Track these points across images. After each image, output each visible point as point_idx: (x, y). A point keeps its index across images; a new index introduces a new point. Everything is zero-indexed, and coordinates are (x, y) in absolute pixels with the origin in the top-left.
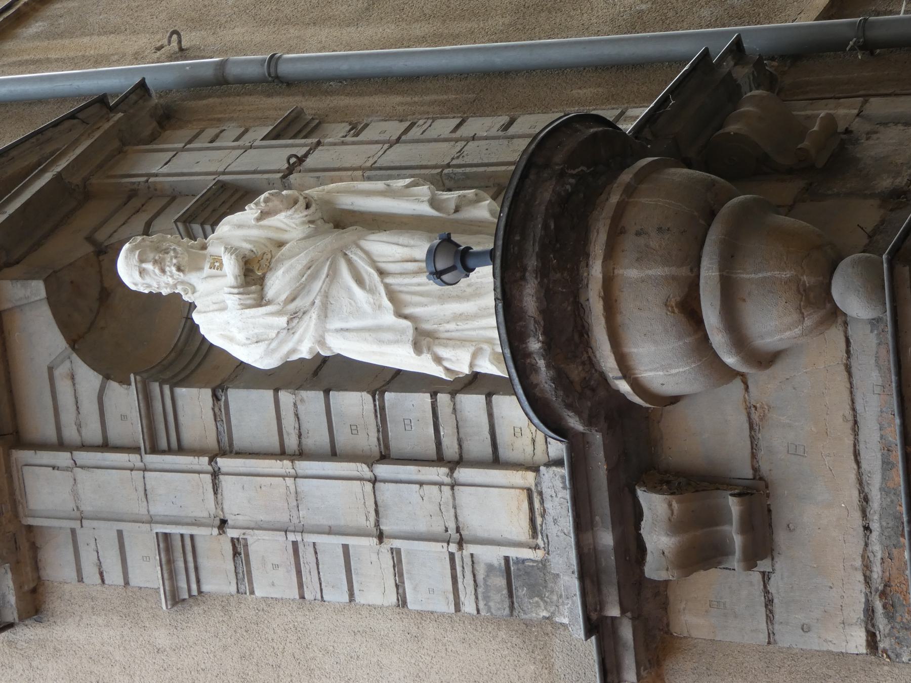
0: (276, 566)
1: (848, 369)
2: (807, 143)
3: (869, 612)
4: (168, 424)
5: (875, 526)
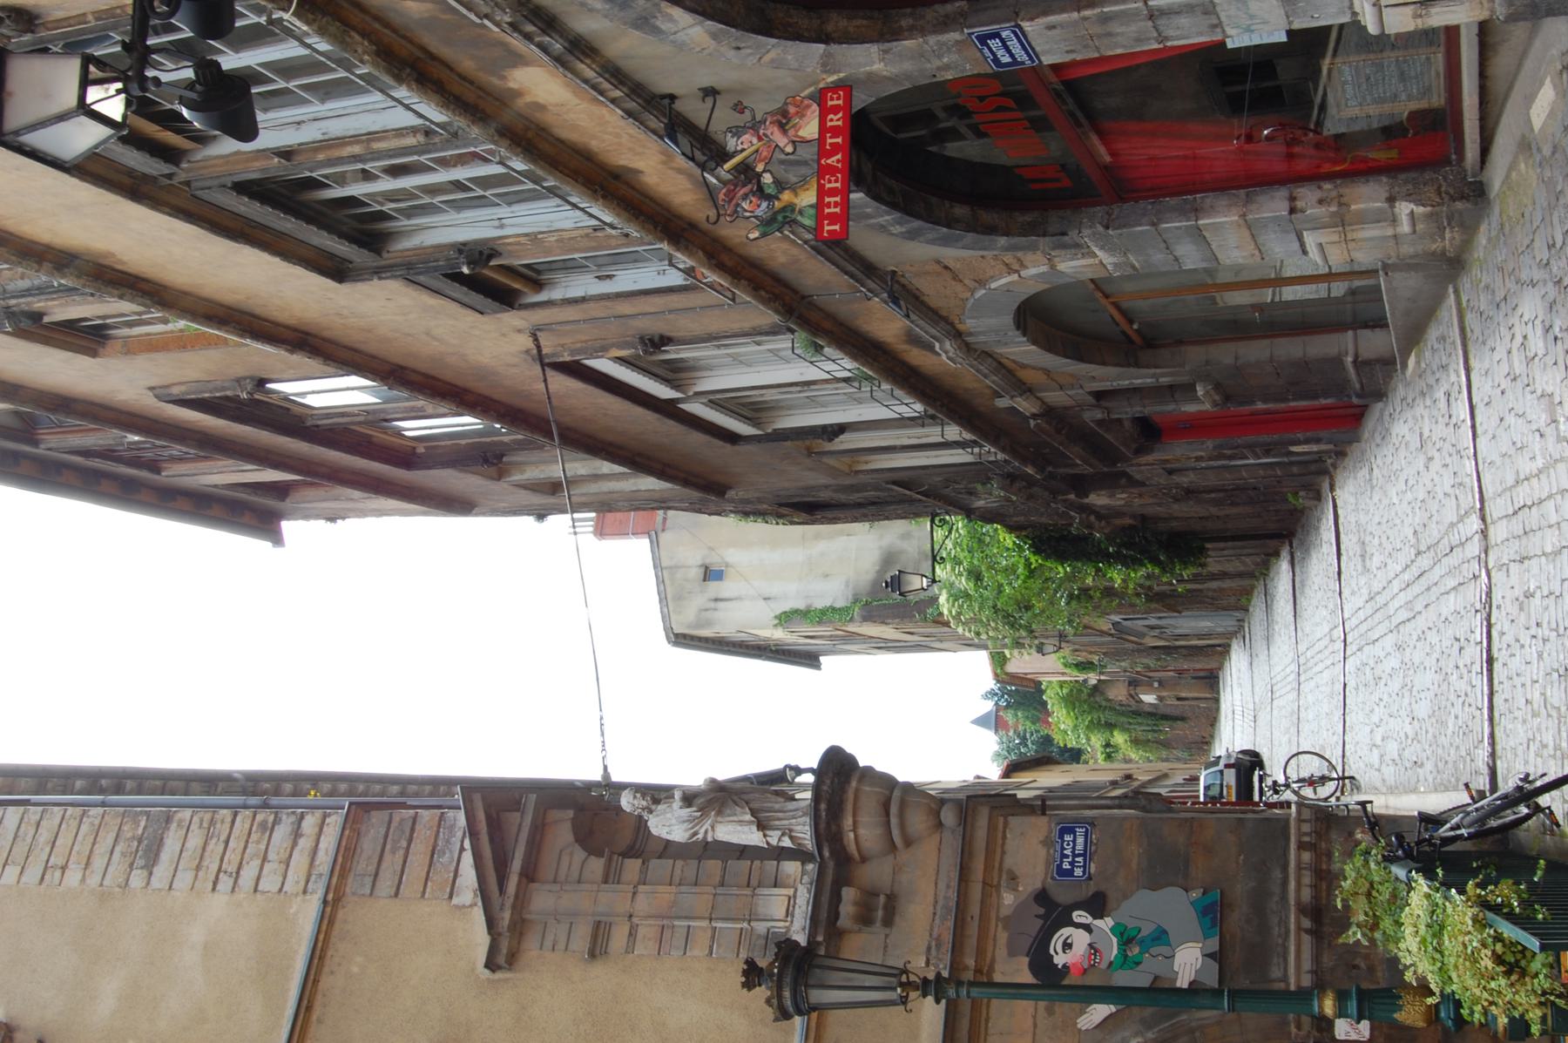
0: (649, 939)
1: (939, 850)
2: (1422, 226)
3: (929, 949)
4: (312, 945)
5: (939, 913)
